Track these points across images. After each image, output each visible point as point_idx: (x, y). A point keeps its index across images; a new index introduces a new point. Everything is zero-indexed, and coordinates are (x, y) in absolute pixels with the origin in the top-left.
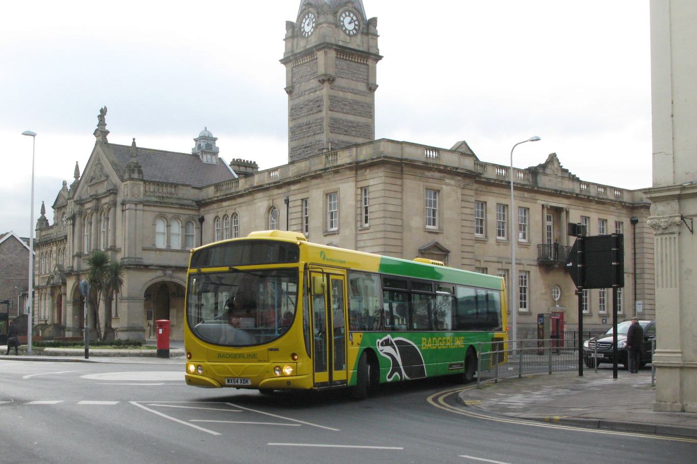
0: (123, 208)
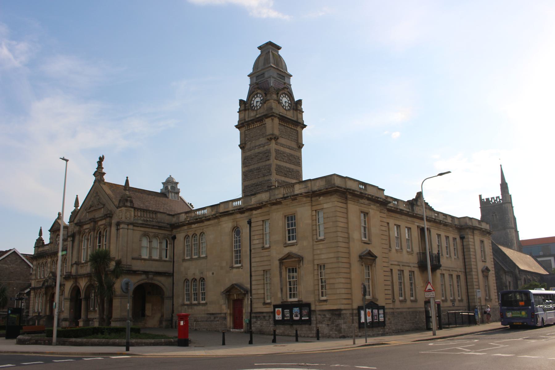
0: (117, 228)
